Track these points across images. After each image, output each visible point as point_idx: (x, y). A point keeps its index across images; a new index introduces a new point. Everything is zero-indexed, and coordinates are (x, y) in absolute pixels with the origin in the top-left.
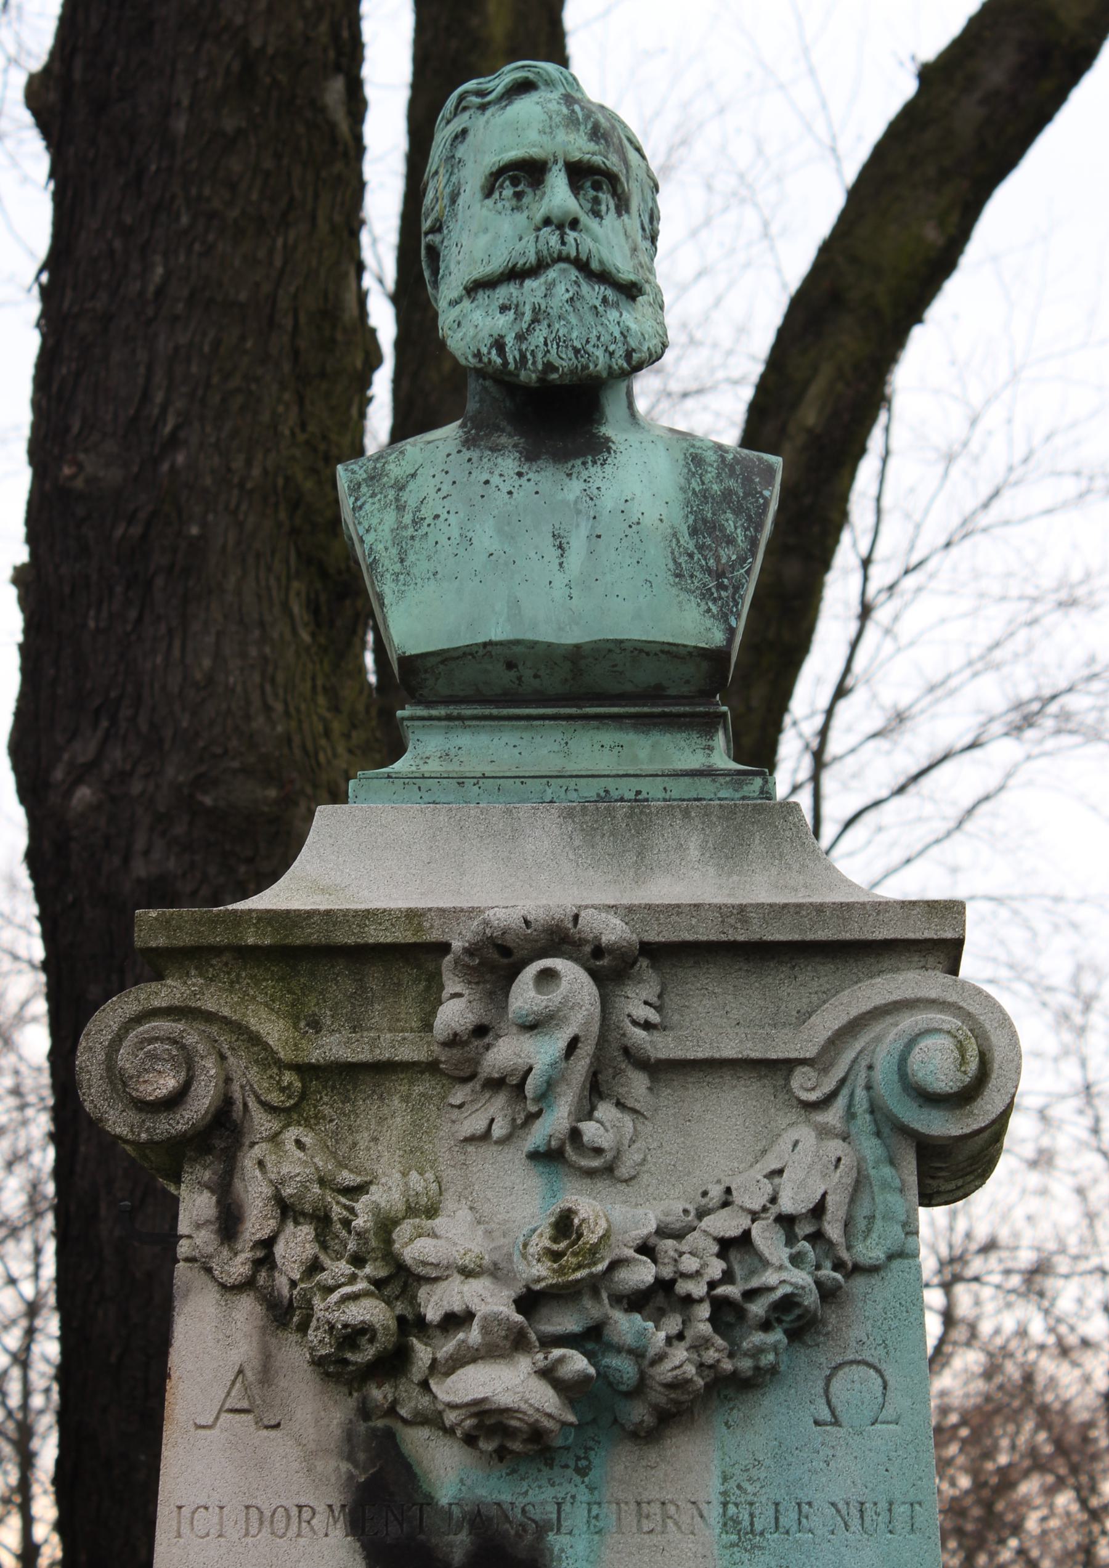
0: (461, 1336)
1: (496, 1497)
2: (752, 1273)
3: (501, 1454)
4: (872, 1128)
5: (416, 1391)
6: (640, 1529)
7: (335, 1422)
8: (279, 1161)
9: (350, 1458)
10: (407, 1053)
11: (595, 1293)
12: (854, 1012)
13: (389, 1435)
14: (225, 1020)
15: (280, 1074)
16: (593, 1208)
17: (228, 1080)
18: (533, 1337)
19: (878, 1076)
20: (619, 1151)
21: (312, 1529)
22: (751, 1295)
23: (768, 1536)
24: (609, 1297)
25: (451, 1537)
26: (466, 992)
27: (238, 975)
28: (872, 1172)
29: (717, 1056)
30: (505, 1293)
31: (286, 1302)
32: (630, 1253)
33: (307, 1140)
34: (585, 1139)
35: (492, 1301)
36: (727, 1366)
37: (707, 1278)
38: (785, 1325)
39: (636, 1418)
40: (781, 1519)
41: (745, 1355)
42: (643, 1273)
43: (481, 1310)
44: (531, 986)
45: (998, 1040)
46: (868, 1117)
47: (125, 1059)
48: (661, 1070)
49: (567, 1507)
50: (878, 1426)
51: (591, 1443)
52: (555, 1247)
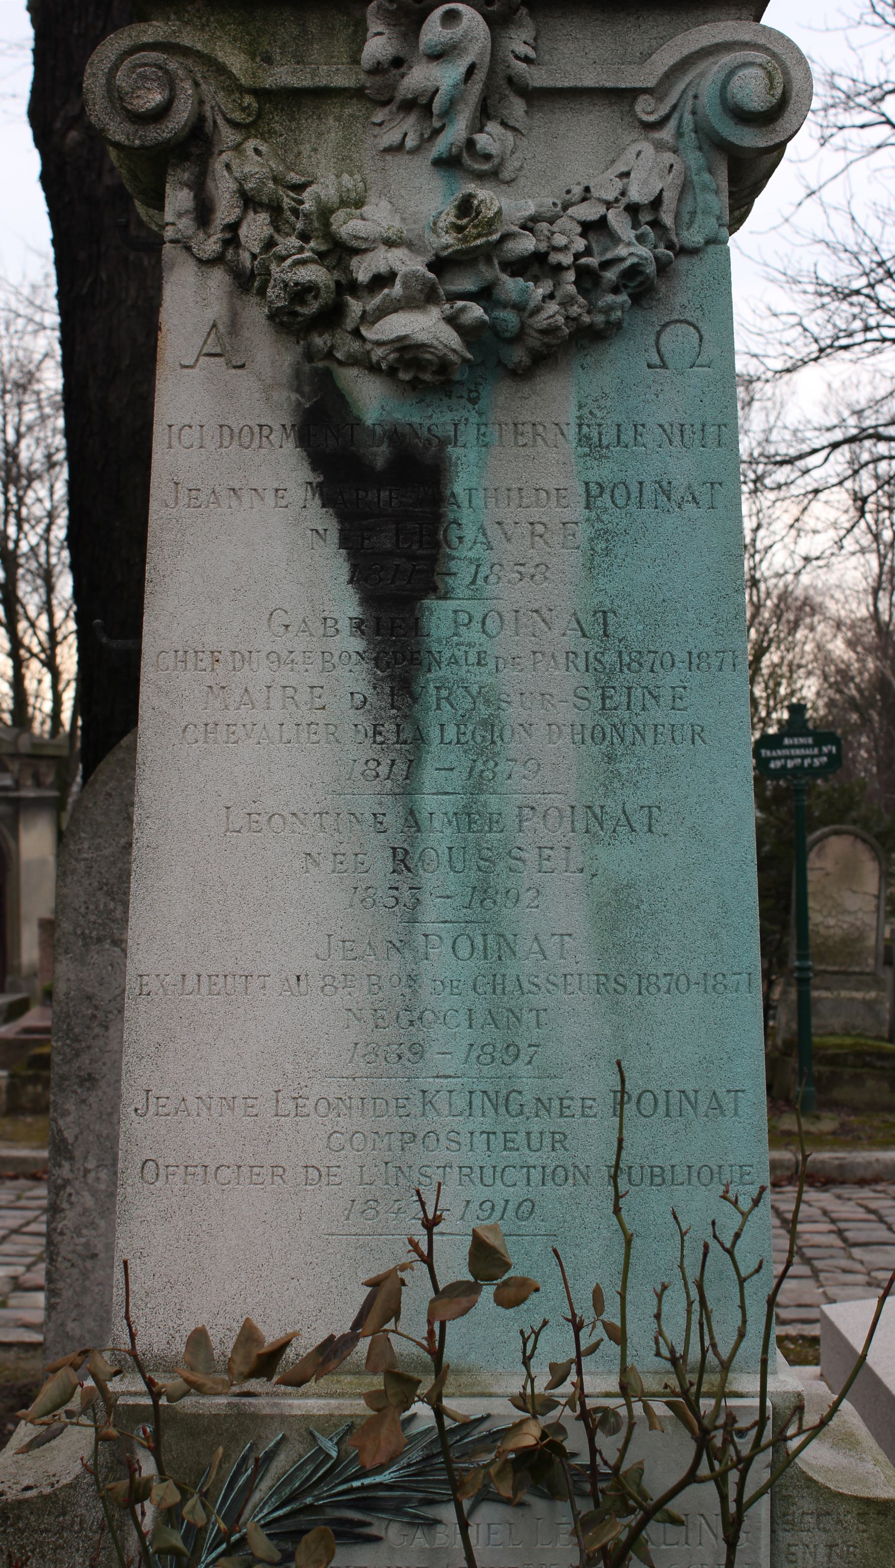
0: (386, 291)
1: (408, 419)
2: (606, 250)
3: (414, 385)
4: (696, 143)
5: (348, 338)
6: (516, 444)
7: (286, 363)
8: (246, 161)
9: (298, 390)
10: (340, 81)
11: (489, 261)
12: (686, 52)
13: (328, 374)
14: (198, 54)
15: (242, 98)
16: (486, 196)
17: (201, 102)
18: (442, 292)
19: (704, 100)
20: (503, 159)
21: (270, 442)
22: (606, 265)
23: (612, 448)
24: (499, 263)
25: (375, 449)
26: (386, 32)
27: (208, 20)
28: (695, 178)
29: (579, 85)
30: (420, 259)
31: (248, 272)
32: (516, 229)
33: (263, 148)
34: (478, 146)
35: (408, 264)
36: (586, 319)
37: (573, 251)
38: (630, 290)
39: (516, 360)
40: (622, 437)
41: (600, 312)
42: (527, 244)
43: (402, 270)
44: (438, 23)
45: (796, 74)
46: (693, 135)
47: (122, 80)
48: (537, 97)
49: (461, 427)
50: (695, 369)
51: (480, 380)
52: (459, 222)
